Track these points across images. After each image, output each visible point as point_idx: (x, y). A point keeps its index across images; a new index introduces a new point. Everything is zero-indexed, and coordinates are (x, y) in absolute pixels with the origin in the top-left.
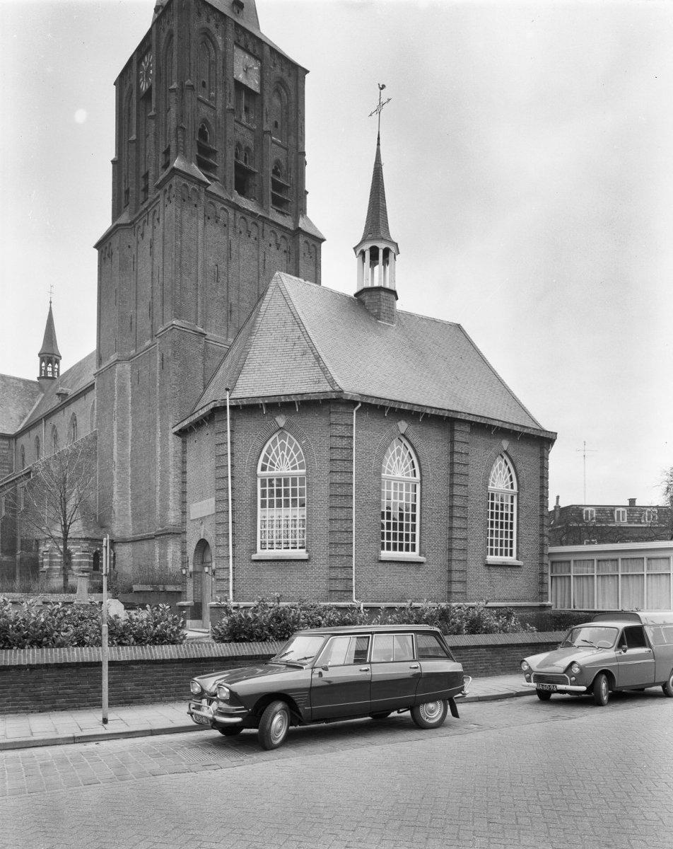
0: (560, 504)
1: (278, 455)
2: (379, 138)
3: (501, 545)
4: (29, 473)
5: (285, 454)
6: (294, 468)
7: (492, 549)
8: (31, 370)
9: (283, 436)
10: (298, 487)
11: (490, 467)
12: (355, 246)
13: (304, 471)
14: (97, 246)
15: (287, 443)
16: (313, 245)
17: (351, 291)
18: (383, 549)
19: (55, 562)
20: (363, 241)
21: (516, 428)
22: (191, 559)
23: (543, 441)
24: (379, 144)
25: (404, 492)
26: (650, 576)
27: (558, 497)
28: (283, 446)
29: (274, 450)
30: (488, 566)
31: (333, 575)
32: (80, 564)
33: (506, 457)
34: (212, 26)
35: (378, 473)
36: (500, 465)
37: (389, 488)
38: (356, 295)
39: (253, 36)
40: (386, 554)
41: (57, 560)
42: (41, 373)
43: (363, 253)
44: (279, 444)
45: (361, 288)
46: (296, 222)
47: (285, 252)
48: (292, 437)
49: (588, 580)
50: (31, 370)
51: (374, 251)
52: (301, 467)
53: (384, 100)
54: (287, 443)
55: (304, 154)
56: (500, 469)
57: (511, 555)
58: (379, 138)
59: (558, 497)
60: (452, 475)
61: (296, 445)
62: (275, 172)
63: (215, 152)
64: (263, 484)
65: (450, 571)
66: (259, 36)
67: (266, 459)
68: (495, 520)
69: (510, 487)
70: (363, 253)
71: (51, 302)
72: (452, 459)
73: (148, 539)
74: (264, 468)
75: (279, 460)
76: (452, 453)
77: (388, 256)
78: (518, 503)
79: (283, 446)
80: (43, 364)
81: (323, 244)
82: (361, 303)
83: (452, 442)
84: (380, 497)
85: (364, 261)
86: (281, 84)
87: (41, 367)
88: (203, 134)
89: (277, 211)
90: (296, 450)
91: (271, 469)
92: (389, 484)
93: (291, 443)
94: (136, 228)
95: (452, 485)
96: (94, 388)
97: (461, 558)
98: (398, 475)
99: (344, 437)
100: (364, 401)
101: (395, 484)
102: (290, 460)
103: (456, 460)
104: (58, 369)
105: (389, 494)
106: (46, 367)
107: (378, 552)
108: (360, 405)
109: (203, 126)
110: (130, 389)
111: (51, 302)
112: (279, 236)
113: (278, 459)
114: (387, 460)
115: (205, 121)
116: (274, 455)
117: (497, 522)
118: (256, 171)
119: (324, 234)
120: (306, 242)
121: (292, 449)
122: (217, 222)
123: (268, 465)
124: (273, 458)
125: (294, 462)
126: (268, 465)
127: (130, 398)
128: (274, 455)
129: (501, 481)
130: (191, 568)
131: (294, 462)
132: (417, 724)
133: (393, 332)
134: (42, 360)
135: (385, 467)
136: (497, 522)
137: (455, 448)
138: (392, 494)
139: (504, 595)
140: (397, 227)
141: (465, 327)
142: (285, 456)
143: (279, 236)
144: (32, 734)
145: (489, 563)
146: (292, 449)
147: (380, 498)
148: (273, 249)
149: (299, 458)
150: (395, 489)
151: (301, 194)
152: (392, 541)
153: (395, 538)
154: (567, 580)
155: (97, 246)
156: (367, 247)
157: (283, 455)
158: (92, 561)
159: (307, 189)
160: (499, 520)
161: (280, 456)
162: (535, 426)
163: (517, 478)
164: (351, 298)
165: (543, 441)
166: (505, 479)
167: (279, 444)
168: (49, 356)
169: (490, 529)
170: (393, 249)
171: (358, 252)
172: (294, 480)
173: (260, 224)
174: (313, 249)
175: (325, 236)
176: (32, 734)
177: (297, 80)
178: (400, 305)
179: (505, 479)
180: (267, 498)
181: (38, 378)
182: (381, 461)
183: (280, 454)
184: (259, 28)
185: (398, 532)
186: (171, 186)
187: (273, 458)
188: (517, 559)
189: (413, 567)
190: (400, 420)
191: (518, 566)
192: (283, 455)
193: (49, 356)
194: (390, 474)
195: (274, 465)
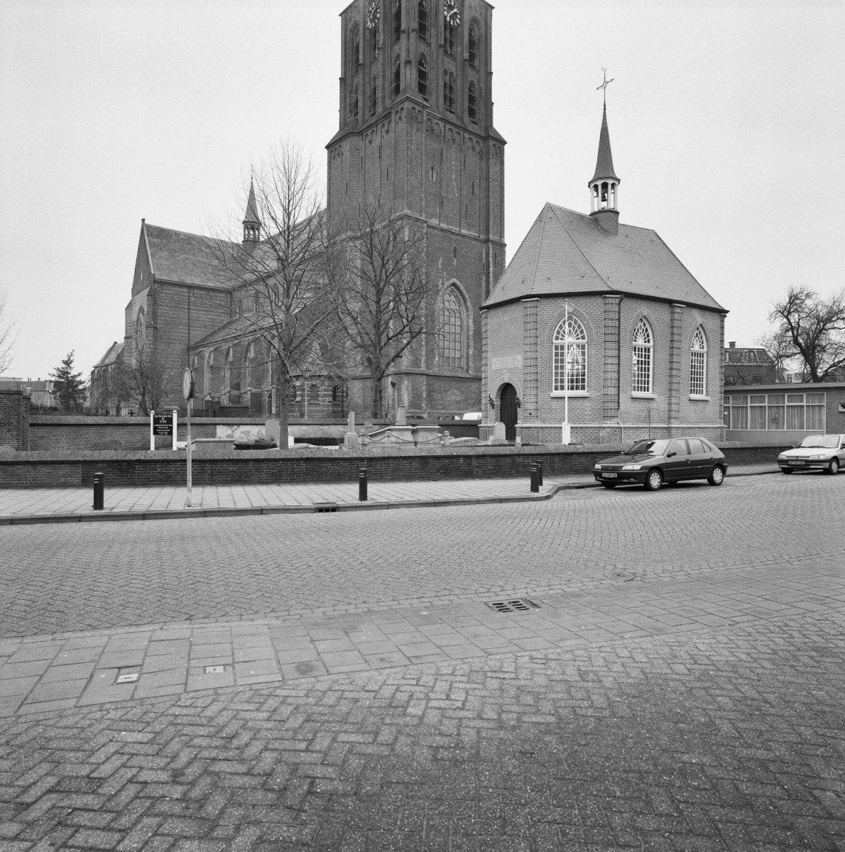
6: (578, 339)
8: (236, 235)
14: (327, 147)
16: (499, 148)
24: (605, 109)
25: (643, 353)
26: (790, 408)
33: (644, 320)
38: (592, 214)
40: (694, 396)
42: (245, 238)
43: (596, 187)
49: (813, 409)
50: (236, 235)
51: (605, 186)
53: (601, 90)
57: (648, 391)
58: (605, 105)
67: (558, 333)
70: (596, 187)
80: (246, 232)
82: (596, 221)
86: (475, 22)
88: (421, 64)
91: (561, 339)
94: (364, 136)
106: (249, 233)
109: (421, 59)
112: (474, 142)
115: (423, 55)
119: (506, 139)
120: (494, 145)
123: (560, 337)
124: (562, 336)
125: (577, 331)
126: (560, 337)
131: (577, 331)
132: (712, 483)
133: (618, 240)
134: (246, 228)
139: (208, 445)
143: (474, 142)
144: (689, 453)
148: (470, 152)
154: (745, 410)
155: (327, 147)
156: (599, 183)
157: (570, 330)
159: (493, 101)
162: (719, 308)
165: (722, 313)
168: (252, 224)
171: (592, 185)
173: (462, 132)
174: (498, 150)
176: (689, 453)
178: (621, 220)
186: (402, 108)
188: (707, 395)
189: (581, 400)
191: (706, 401)
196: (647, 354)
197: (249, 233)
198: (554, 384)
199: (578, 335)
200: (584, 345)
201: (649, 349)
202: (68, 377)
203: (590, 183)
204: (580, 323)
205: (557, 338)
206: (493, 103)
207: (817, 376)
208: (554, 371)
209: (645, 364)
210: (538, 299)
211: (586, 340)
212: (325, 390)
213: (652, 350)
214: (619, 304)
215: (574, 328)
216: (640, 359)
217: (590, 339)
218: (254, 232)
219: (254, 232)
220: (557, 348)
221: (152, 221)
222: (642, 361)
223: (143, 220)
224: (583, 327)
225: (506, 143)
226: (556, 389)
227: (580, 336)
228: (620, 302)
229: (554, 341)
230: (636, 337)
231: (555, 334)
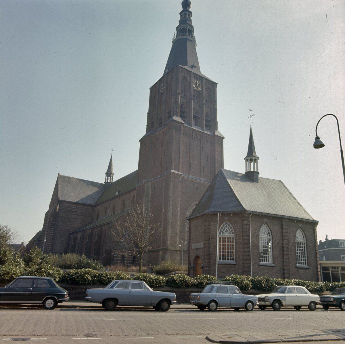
0: (328, 238)
3: (302, 261)
4: (110, 223)
6: (230, 234)
7: (298, 262)
9: (226, 223)
10: (232, 240)
11: (295, 233)
17: (243, 172)
18: (260, 261)
19: (118, 259)
20: (247, 157)
21: (303, 220)
22: (192, 262)
23: (314, 224)
27: (327, 236)
28: (226, 227)
30: (297, 268)
31: (244, 270)
32: (128, 260)
34: (186, 75)
35: (258, 236)
36: (299, 232)
37: (262, 240)
39: (199, 76)
41: (119, 259)
42: (106, 181)
46: (214, 133)
47: (210, 143)
48: (232, 226)
50: (101, 179)
52: (233, 233)
53: (252, 115)
55: (217, 110)
57: (306, 264)
58: (251, 125)
59: (327, 236)
60: (282, 236)
61: (229, 224)
62: (206, 116)
63: (186, 112)
65: (283, 240)
66: (201, 75)
69: (303, 240)
71: (112, 154)
72: (282, 231)
73: (156, 251)
76: (282, 229)
78: (307, 245)
79: (226, 227)
80: (107, 177)
81: (224, 140)
83: (282, 225)
84: (259, 244)
87: (106, 178)
89: (207, 129)
90: (231, 228)
91: (223, 234)
92: (262, 239)
93: (229, 225)
95: (283, 240)
96: (135, 190)
97: (287, 265)
98: (265, 236)
99: (247, 224)
100: (253, 213)
101: (264, 240)
103: (283, 231)
104: (112, 179)
105: (262, 242)
107: (259, 262)
108: (252, 214)
110: (150, 192)
111: (112, 154)
113: (225, 231)
114: (261, 231)
118: (200, 117)
119: (224, 136)
121: (229, 228)
122: (186, 135)
123: (222, 232)
124: (223, 230)
125: (230, 230)
126: (222, 232)
127: (150, 196)
129: (300, 237)
130: (192, 265)
131: (230, 230)
135: (260, 234)
137: (285, 275)
138: (263, 243)
140: (258, 152)
141: (283, 182)
145: (298, 267)
146: (229, 228)
147: (259, 244)
149: (232, 230)
150: (264, 241)
151: (216, 123)
152: (263, 259)
153: (264, 258)
157: (226, 229)
158: (132, 259)
161: (226, 230)
162: (312, 220)
163: (306, 237)
164: (244, 175)
165: (314, 224)
168: (109, 173)
171: (246, 160)
172: (230, 238)
175: (225, 137)
177: (214, 87)
180: (229, 247)
181: (104, 183)
182: (259, 232)
184: (200, 72)
185: (265, 255)
188: (308, 266)
190: (264, 218)
192: (226, 229)
193: (109, 173)
194: (262, 236)
195: (223, 233)
197: (108, 178)
200: (234, 237)
206: (218, 122)
207: (325, 257)
209: (303, 251)
212: (128, 257)
215: (228, 228)
216: (265, 245)
218: (110, 178)
219: (110, 178)
221: (62, 174)
222: (266, 246)
223: (59, 173)
227: (231, 232)
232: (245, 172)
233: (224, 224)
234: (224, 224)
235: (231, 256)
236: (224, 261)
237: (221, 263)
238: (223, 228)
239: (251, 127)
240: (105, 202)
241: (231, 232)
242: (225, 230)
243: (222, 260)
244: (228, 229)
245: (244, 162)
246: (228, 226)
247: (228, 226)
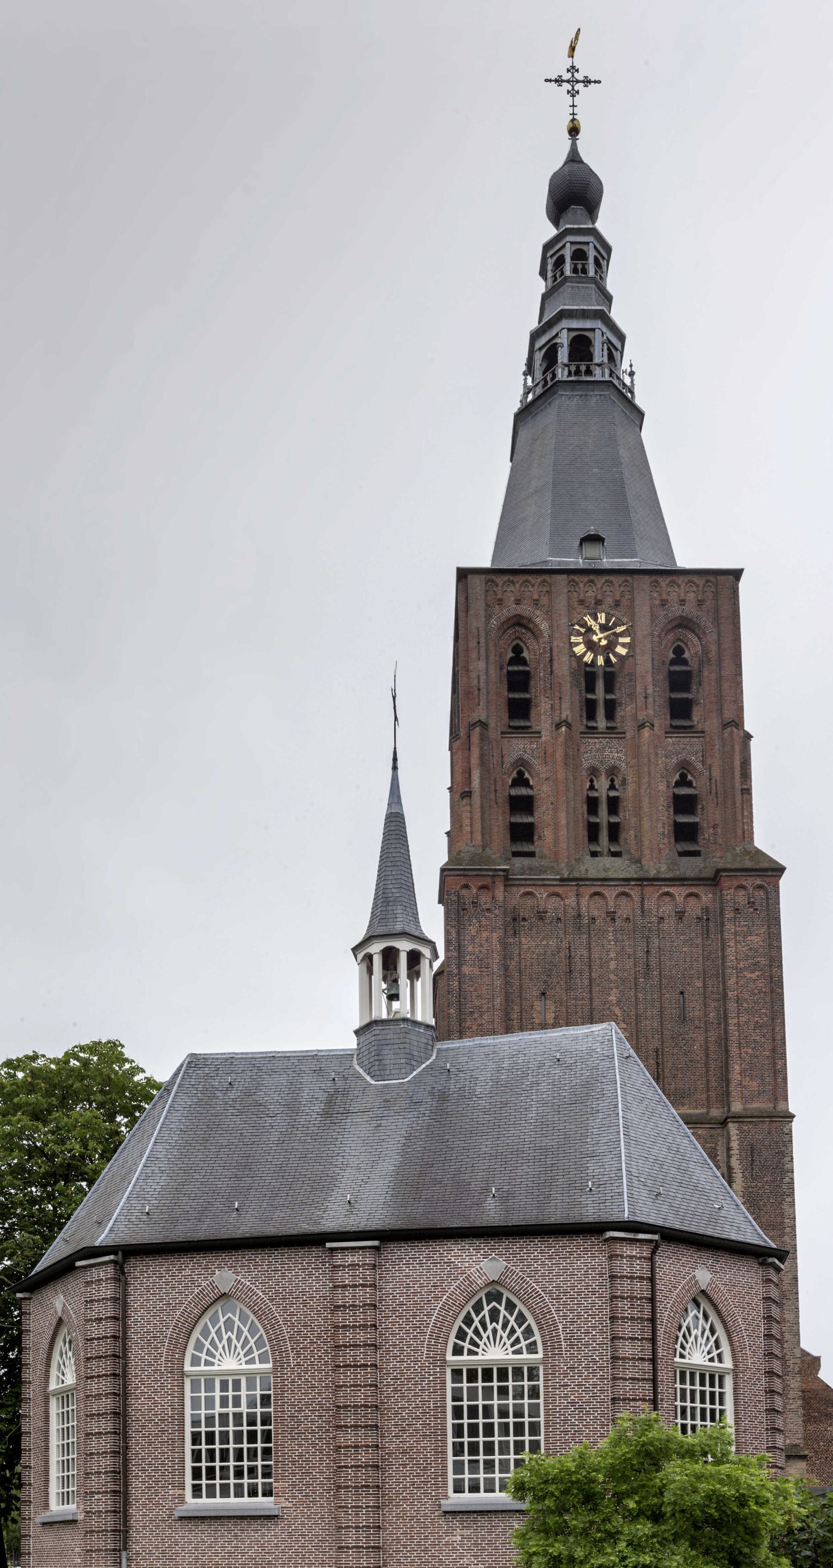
1: (485, 1329)
2: (395, 759)
5: (234, 1337)
12: (354, 946)
13: (270, 1366)
14: (440, 902)
15: (236, 1319)
24: (395, 768)
28: (229, 1324)
29: (213, 1331)
33: (704, 1304)
43: (369, 958)
44: (222, 1320)
45: (367, 1021)
51: (390, 957)
52: (263, 1359)
54: (236, 1319)
56: (697, 1327)
58: (395, 759)
64: (195, 1387)
67: (461, 1335)
68: (689, 1422)
74: (196, 1361)
75: (224, 1348)
77: (419, 963)
79: (229, 1324)
85: (370, 971)
91: (471, 1352)
93: (243, 1319)
102: (243, 1348)
113: (220, 1346)
116: (476, 1328)
117: (693, 1409)
123: (203, 1356)
124: (473, 1343)
125: (246, 1341)
126: (203, 1356)
128: (476, 1328)
131: (246, 1341)
136: (693, 1409)
142: (235, 1341)
146: (245, 1330)
156: (376, 948)
157: (229, 1340)
160: (707, 1389)
161: (225, 1342)
166: (706, 1345)
167: (222, 1320)
169: (678, 1403)
170: (426, 952)
171: (360, 956)
172: (518, 1372)
179: (706, 1345)
183: (225, 1337)
187: (213, 1343)
192: (229, 1340)
195: (214, 1356)
196: (717, 1389)
198: (451, 1477)
199: (517, 1341)
200: (537, 1368)
201: (721, 1378)
202: (18, 1411)
203: (355, 950)
204: (256, 1322)
205: (458, 1351)
208: (450, 1440)
210: (376, 1243)
211: (540, 1355)
213: (729, 1382)
214: (651, 1260)
215: (240, 1333)
217: (551, 1346)
220: (457, 1374)
224: (531, 1320)
225: (779, 870)
226: (458, 1489)
228: (653, 1252)
229: (450, 1357)
230: (683, 1347)
231: (452, 1340)
232: (20, 1057)
233: (480, 1301)
234: (480, 1301)
235: (474, 1464)
236: (246, 1500)
237: (463, 1509)
238: (213, 1334)
239: (395, 748)
240: (590, 958)
241: (256, 1354)
242: (481, 1338)
243: (236, 1496)
244: (238, 1339)
245: (353, 969)
246: (502, 1309)
247: (502, 1309)
